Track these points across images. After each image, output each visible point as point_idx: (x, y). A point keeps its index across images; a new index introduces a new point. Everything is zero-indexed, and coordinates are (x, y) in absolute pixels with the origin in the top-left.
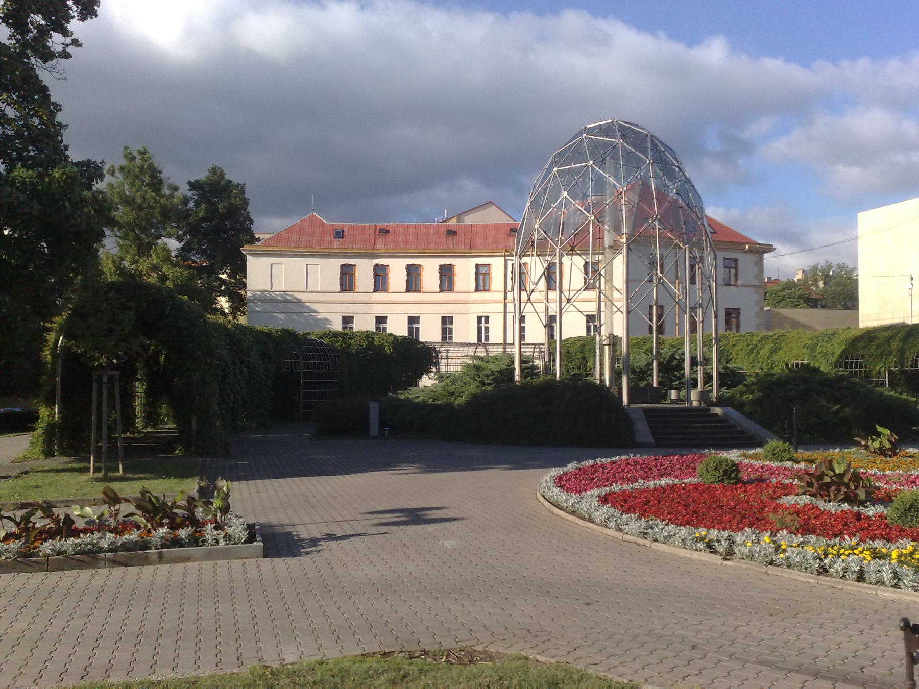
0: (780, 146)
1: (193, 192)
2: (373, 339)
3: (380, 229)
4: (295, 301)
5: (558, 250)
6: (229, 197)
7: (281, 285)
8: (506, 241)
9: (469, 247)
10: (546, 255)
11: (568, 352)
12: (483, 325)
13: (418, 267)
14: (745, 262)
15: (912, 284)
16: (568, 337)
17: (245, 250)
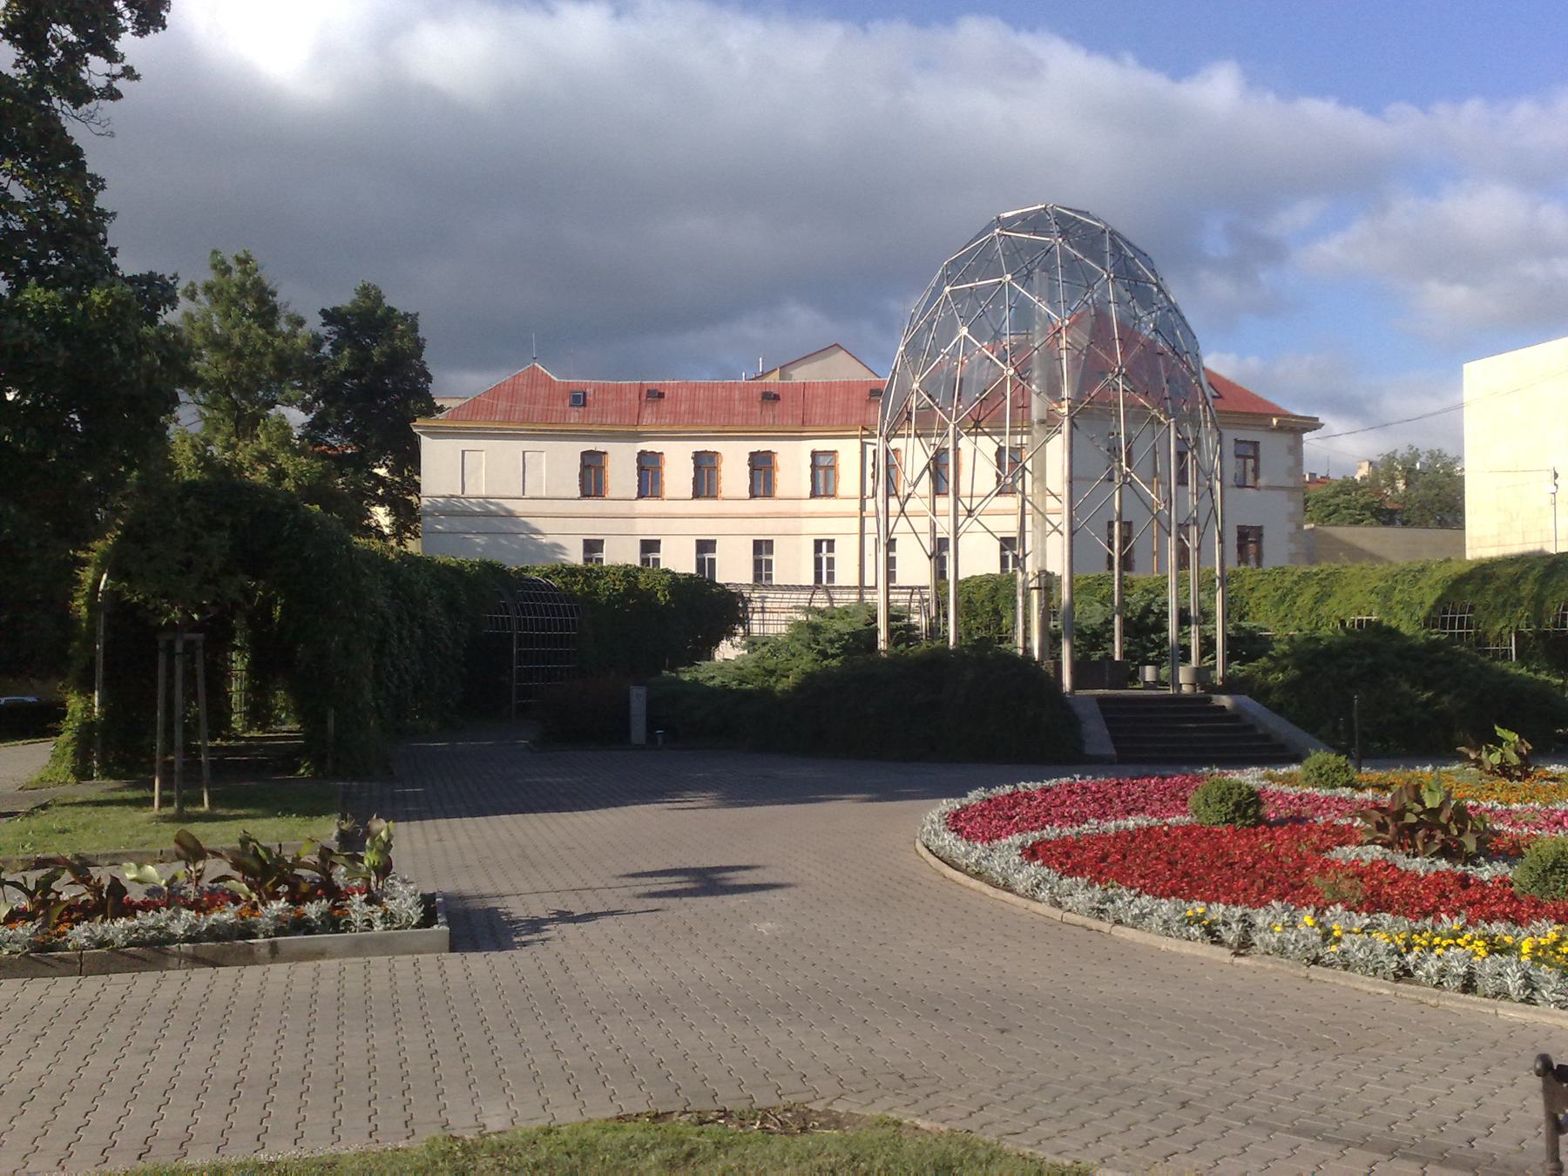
0: (1330, 250)
2: (636, 578)
3: (648, 391)
4: (503, 514)
5: (952, 426)
6: (391, 337)
7: (479, 487)
8: (863, 412)
9: (800, 421)
10: (931, 435)
11: (969, 601)
12: (824, 555)
13: (714, 455)
14: (1272, 447)
15: (1555, 485)
16: (969, 576)
17: (418, 427)
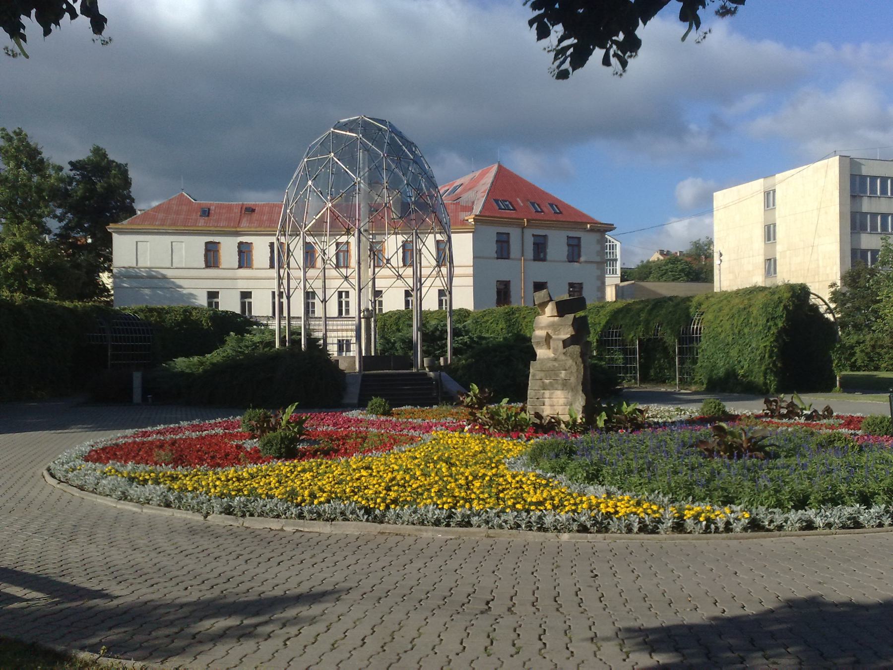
0: (763, 123)
1: (74, 172)
2: (191, 313)
3: (246, 208)
4: (160, 277)
6: (109, 178)
7: (146, 262)
10: (322, 235)
12: (344, 299)
13: (249, 245)
14: (588, 242)
17: (109, 228)
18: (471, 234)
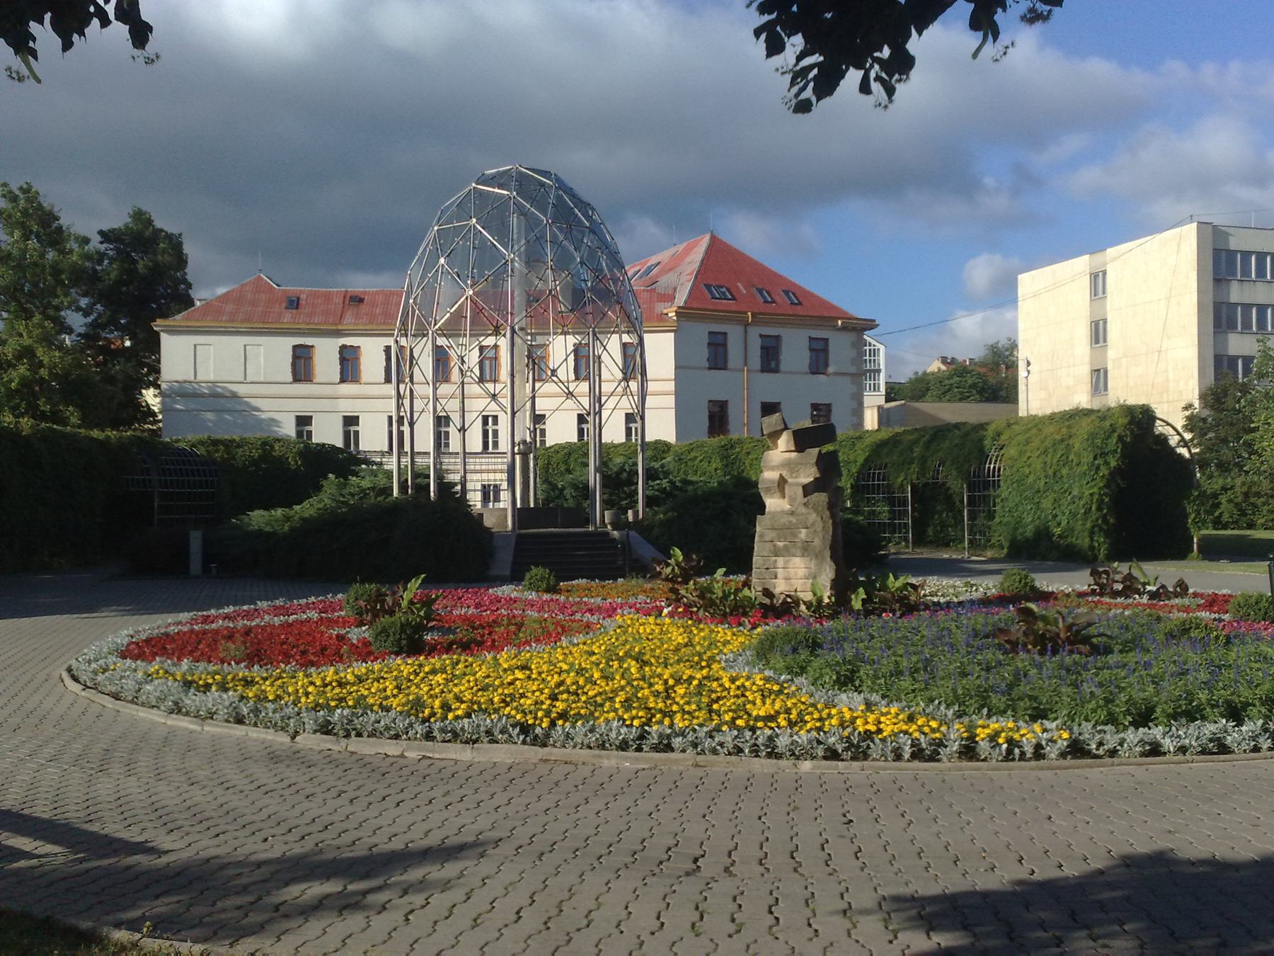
2: (272, 447)
3: (351, 297)
4: (228, 395)
6: (155, 254)
7: (208, 373)
10: (459, 335)
12: (490, 427)
13: (356, 349)
14: (839, 345)
17: (156, 326)
18: (673, 334)
